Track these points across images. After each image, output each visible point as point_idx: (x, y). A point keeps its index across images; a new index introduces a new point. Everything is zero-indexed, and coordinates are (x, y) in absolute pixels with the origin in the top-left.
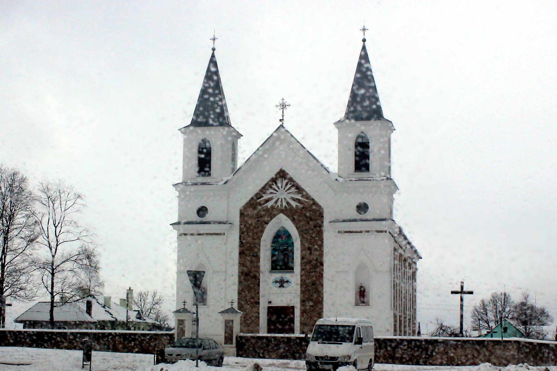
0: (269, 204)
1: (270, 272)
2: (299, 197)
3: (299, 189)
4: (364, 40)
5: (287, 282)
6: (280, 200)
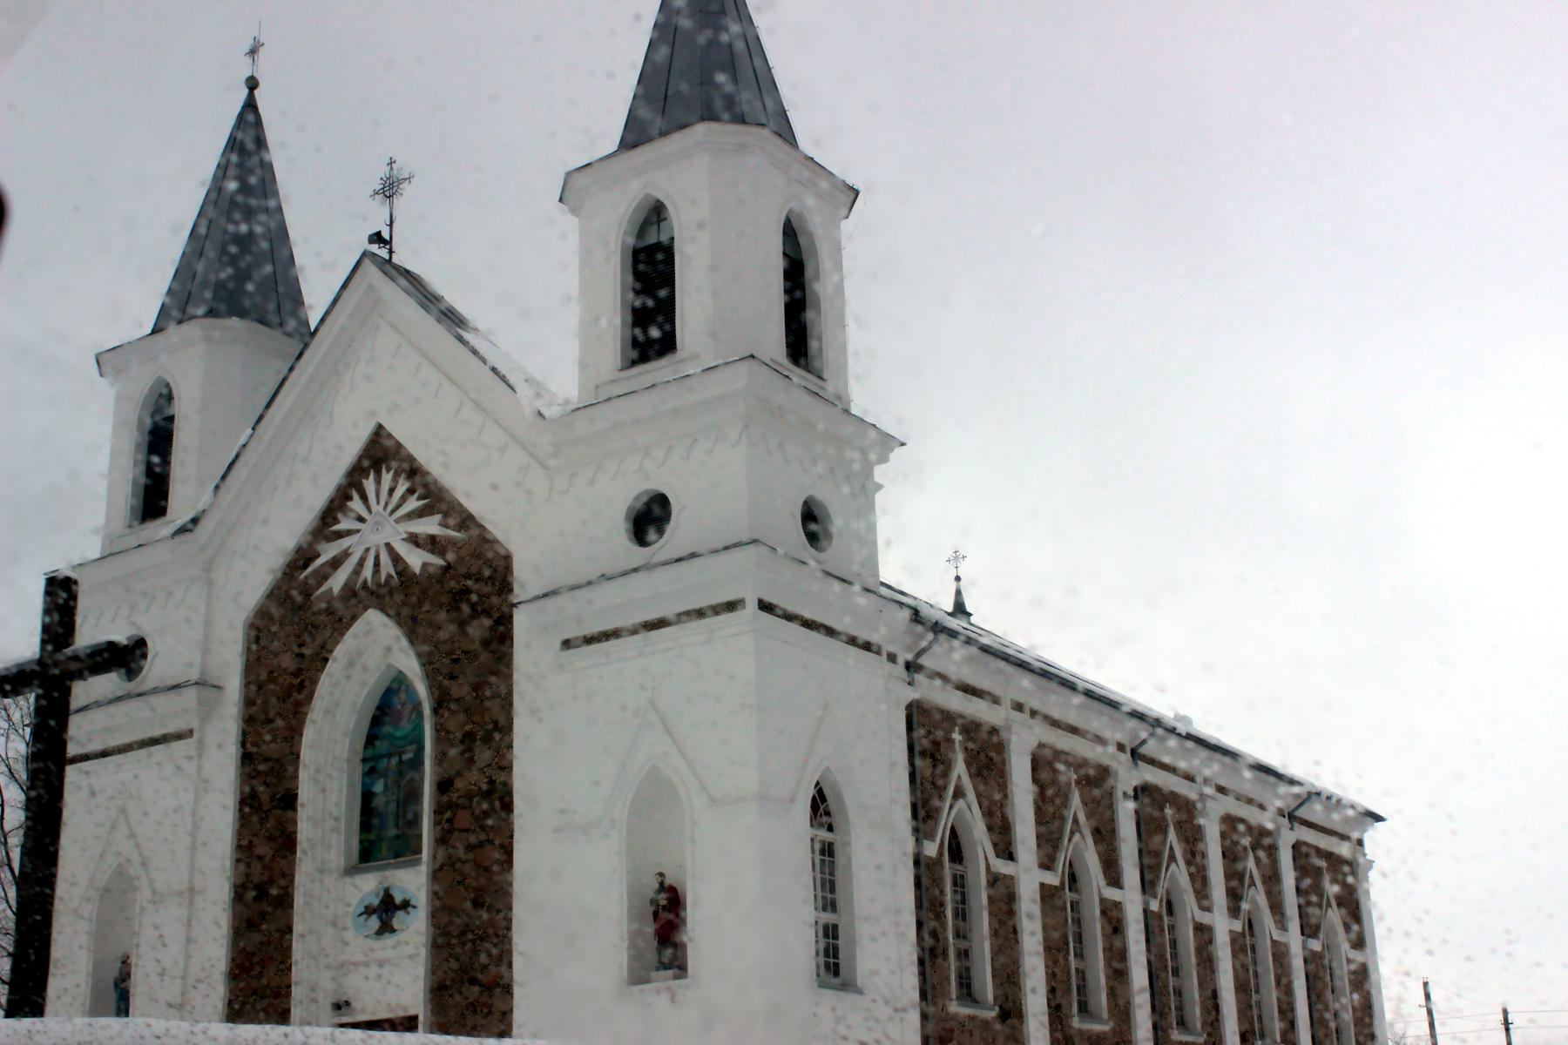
3: (435, 499)
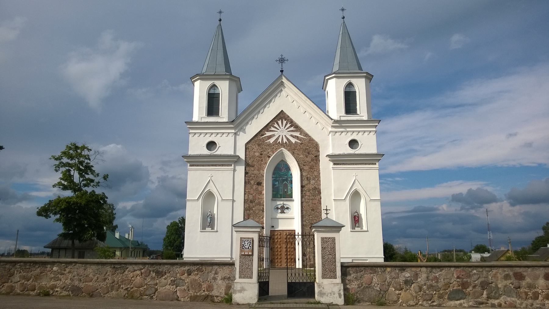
0: (272, 140)
1: (272, 200)
2: (297, 134)
3: (297, 128)
4: (220, 20)
5: (287, 208)
6: (281, 137)
